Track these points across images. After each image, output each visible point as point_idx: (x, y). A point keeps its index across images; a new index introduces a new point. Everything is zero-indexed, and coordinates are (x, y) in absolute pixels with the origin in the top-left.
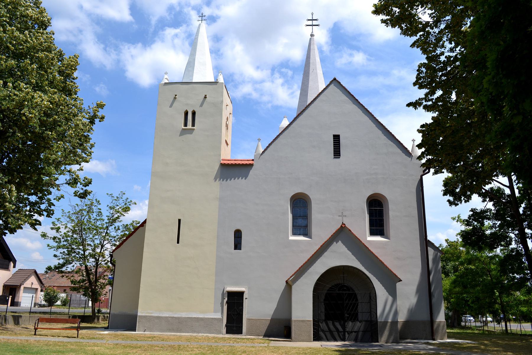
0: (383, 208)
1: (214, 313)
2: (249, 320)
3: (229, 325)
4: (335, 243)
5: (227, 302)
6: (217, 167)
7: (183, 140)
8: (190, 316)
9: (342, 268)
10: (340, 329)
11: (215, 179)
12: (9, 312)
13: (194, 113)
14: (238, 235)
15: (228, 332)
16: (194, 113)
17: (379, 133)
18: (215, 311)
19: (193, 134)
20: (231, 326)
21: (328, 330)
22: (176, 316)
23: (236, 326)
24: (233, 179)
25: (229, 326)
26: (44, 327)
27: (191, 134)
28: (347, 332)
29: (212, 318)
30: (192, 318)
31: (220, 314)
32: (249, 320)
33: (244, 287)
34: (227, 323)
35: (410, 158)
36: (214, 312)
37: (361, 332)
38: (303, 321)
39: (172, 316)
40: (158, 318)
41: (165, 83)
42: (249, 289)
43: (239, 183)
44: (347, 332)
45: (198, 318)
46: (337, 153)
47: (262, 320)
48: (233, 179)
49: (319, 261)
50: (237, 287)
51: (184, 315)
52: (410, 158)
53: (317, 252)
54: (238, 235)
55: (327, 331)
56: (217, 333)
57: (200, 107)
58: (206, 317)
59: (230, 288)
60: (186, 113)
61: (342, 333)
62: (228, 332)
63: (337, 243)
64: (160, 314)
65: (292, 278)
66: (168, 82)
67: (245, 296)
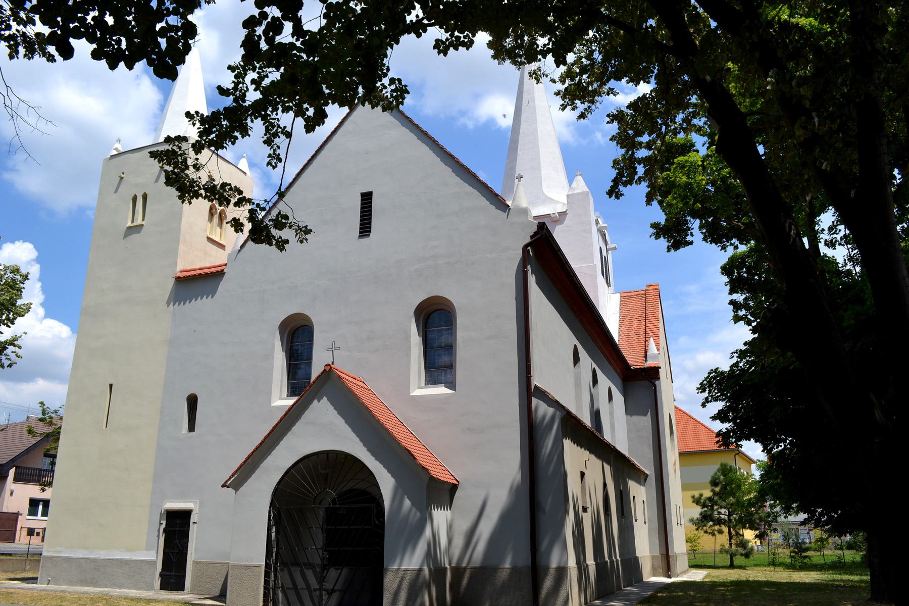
0: (452, 326)
1: (146, 552)
2: (195, 563)
3: (165, 573)
4: (316, 401)
5: (165, 531)
6: (172, 281)
7: (127, 248)
8: (111, 557)
9: (343, 456)
10: (314, 584)
11: (168, 303)
12: (30, 554)
13: (145, 197)
14: (192, 402)
15: (163, 587)
16: (145, 197)
17: (446, 172)
18: (148, 548)
19: (142, 232)
20: (168, 575)
21: (292, 587)
22: (92, 556)
23: (176, 576)
24: (194, 299)
25: (164, 575)
26: (339, 582)
27: (139, 232)
28: (326, 590)
29: (142, 561)
30: (113, 560)
31: (154, 552)
32: (195, 563)
33: (191, 502)
34: (162, 569)
35: (505, 212)
36: (146, 550)
37: (338, 593)
38: (247, 567)
39: (86, 556)
40: (67, 559)
41: (111, 156)
42: (201, 504)
43: (202, 306)
44: (326, 590)
45: (121, 561)
46: (365, 228)
47: (217, 565)
48: (194, 299)
49: (283, 443)
50: (181, 502)
51: (103, 555)
52: (505, 212)
53: (283, 421)
54: (192, 402)
55: (291, 589)
56: (147, 589)
57: (156, 183)
58: (134, 558)
59: (171, 504)
60: (135, 199)
61: (318, 593)
62: (163, 587)
63: (319, 401)
64: (71, 553)
65: (232, 479)
66: (117, 153)
67: (194, 518)
